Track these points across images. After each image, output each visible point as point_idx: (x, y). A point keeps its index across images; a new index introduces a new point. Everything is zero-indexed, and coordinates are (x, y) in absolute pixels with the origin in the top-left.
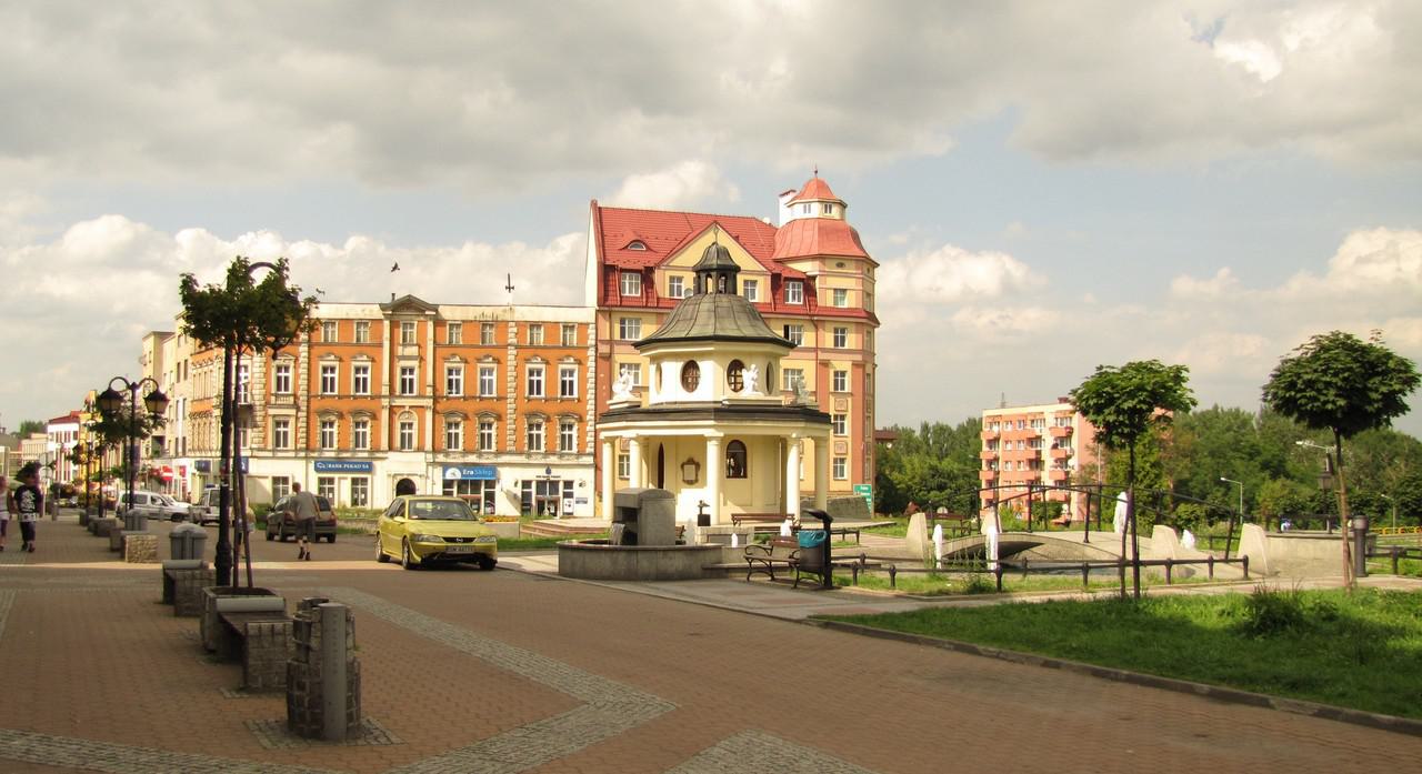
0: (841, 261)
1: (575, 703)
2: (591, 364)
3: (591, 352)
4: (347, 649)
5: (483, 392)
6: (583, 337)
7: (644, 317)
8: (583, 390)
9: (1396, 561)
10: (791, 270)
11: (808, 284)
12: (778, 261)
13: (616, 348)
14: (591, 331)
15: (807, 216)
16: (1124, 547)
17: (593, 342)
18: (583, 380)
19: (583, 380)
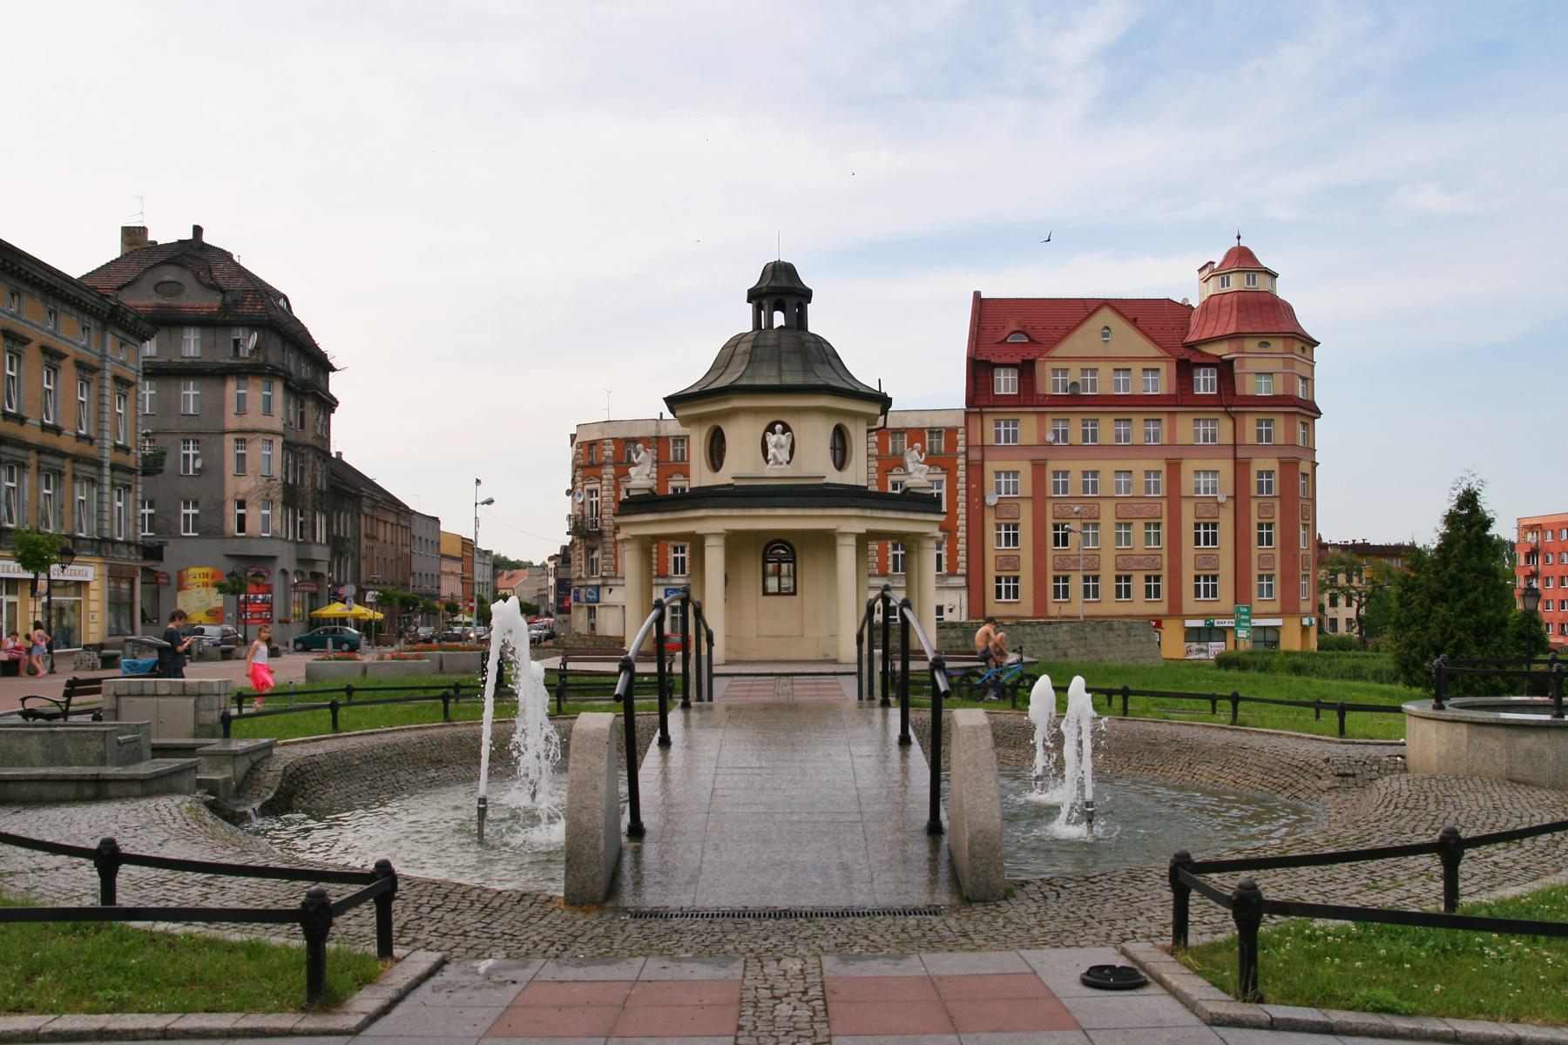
0: (1264, 338)
1: (493, 848)
2: (961, 474)
3: (961, 461)
4: (1450, 849)
5: (1056, 491)
6: (952, 444)
7: (1022, 418)
8: (953, 504)
9: (446, 703)
10: (1204, 354)
11: (1225, 370)
12: (1191, 346)
13: (988, 454)
14: (961, 437)
15: (1226, 289)
16: (318, 707)
17: (963, 449)
18: (953, 492)
19: (953, 492)
